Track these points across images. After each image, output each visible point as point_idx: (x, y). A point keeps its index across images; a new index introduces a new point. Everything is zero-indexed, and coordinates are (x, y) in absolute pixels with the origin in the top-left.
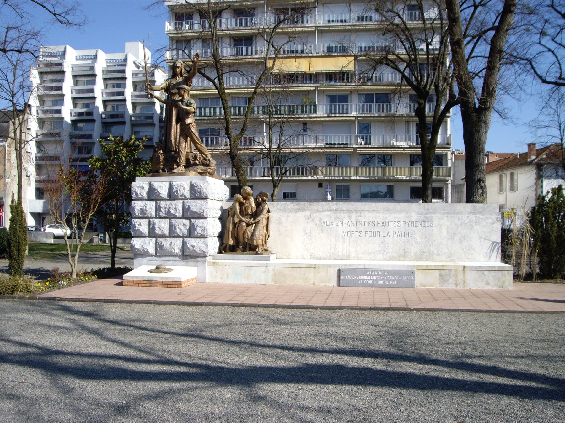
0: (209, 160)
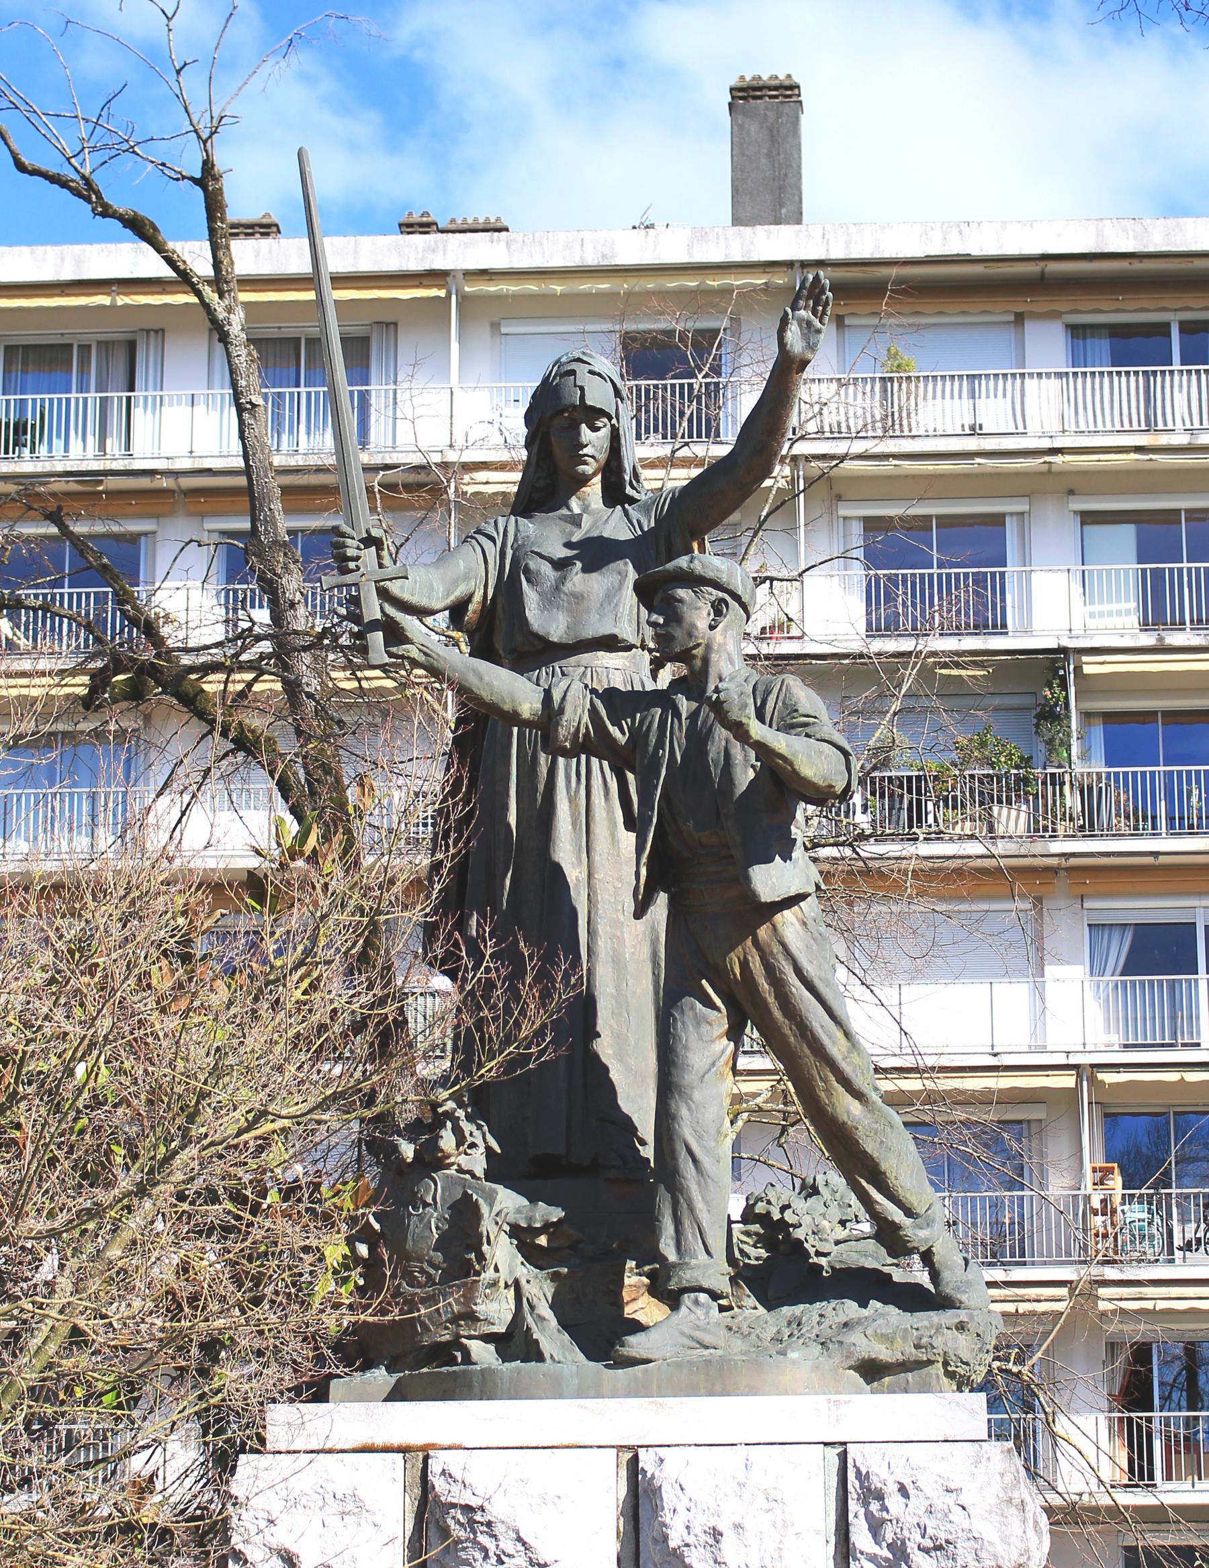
0: (927, 1258)
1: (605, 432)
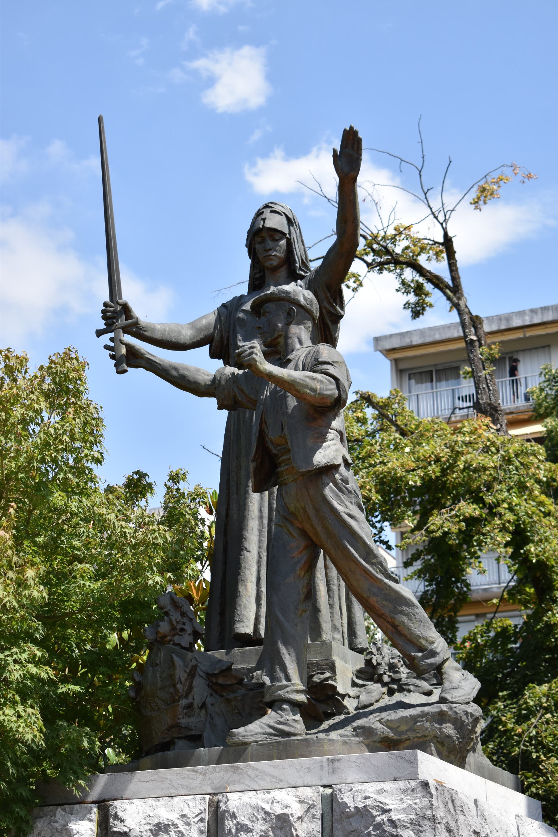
1: (283, 242)
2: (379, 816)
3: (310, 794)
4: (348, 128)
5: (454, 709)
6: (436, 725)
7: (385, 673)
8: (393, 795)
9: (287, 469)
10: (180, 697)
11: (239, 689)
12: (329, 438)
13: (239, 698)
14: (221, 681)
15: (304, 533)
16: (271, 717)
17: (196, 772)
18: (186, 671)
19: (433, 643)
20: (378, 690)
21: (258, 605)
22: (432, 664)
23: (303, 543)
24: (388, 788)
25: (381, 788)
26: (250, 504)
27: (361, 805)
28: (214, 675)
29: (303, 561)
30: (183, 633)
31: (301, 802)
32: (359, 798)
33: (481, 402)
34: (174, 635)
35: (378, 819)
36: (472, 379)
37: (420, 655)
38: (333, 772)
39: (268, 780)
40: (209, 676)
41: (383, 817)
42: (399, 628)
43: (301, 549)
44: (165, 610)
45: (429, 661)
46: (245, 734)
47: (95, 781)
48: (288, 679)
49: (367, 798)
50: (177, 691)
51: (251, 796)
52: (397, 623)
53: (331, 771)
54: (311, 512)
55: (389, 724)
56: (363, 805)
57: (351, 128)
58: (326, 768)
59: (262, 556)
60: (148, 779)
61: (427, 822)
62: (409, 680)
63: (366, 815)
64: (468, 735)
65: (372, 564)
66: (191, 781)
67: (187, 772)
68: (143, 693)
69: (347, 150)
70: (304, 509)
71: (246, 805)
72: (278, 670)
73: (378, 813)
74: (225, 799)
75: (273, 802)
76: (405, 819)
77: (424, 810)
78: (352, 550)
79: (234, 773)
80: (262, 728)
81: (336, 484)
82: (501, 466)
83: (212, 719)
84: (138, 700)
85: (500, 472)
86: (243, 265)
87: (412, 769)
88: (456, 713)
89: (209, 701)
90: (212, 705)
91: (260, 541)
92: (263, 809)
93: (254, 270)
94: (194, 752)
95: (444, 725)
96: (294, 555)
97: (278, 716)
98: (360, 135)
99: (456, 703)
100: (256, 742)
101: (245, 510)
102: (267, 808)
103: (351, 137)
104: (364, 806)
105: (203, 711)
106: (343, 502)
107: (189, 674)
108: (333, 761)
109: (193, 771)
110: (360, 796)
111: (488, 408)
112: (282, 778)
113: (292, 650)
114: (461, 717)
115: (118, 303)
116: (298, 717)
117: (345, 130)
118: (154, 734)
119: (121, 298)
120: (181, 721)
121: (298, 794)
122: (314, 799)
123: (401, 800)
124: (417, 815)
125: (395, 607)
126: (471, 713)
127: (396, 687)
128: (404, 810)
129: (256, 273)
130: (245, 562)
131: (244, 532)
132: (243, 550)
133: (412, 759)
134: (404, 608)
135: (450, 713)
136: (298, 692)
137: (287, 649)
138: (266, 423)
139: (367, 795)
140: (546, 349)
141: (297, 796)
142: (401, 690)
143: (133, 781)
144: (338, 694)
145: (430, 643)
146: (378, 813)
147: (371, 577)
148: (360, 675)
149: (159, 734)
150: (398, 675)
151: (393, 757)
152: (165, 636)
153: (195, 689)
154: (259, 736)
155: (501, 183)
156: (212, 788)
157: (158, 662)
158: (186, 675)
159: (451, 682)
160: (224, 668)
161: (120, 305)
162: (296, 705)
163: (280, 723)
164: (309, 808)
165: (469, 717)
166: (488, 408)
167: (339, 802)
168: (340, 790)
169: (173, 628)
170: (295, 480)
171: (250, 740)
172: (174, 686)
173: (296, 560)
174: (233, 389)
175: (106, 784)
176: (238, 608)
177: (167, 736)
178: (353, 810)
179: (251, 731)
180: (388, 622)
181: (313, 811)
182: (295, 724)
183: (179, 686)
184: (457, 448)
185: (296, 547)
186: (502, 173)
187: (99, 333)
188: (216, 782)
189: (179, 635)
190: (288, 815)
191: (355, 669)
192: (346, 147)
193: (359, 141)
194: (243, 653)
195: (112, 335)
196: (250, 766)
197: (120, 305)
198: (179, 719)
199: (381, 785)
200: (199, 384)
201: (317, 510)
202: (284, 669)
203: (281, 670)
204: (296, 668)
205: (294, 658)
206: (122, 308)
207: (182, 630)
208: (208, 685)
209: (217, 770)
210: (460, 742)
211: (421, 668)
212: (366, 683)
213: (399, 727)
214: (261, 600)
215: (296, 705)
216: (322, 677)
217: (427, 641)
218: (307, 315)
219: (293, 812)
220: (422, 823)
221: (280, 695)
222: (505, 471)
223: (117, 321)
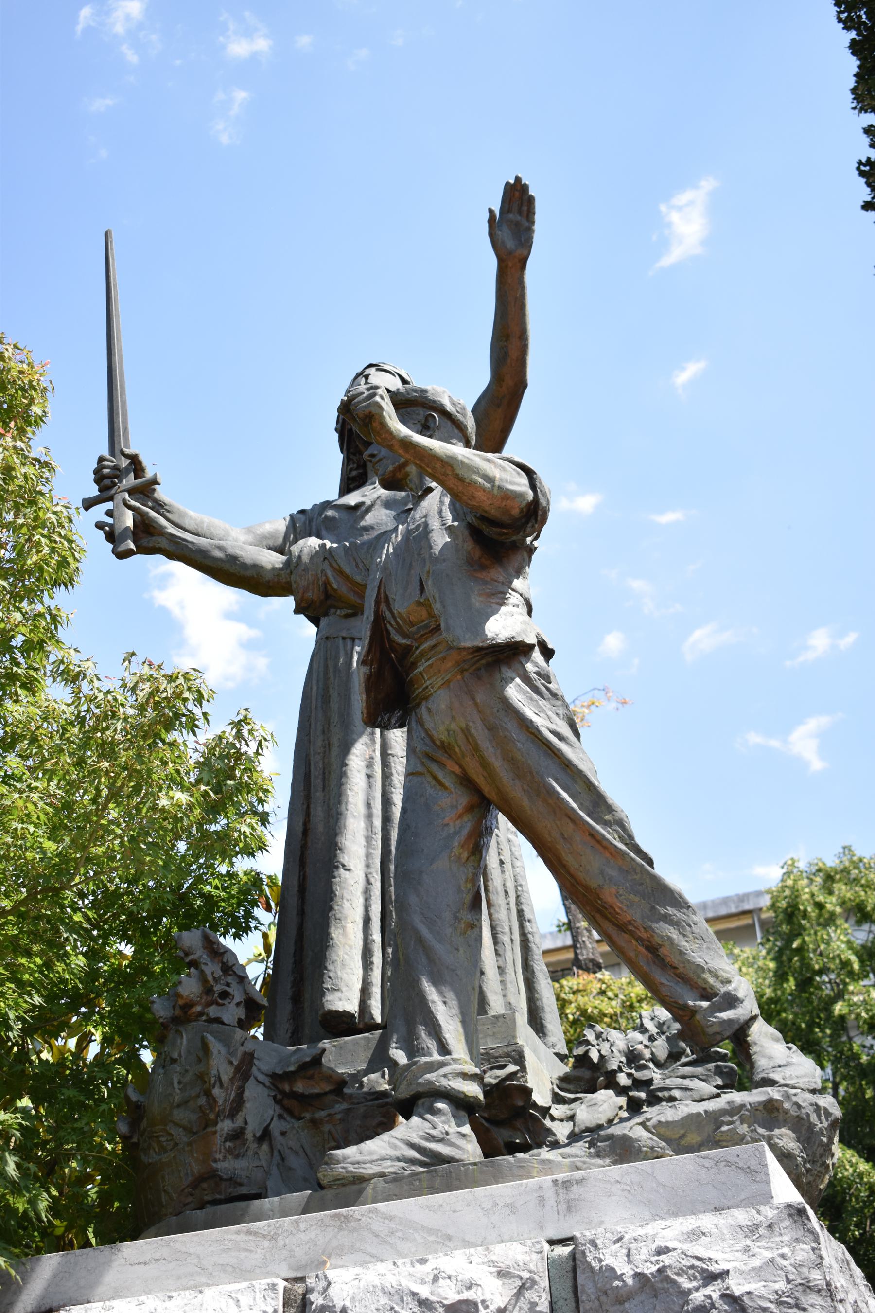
2: (697, 1289)
3: (521, 1258)
4: (512, 181)
5: (794, 1099)
6: (761, 1131)
7: (620, 1070)
8: (723, 1240)
9: (431, 666)
10: (218, 1115)
11: (337, 1102)
12: (511, 601)
13: (338, 1117)
14: (300, 1087)
15: (467, 782)
16: (411, 1129)
17: (255, 1234)
18: (231, 1063)
19: (729, 982)
20: (611, 1101)
21: (367, 964)
22: (730, 1021)
23: (463, 800)
24: (709, 1226)
25: (691, 1227)
26: (349, 792)
27: (650, 1269)
28: (288, 1076)
29: (465, 832)
30: (225, 1002)
31: (502, 1274)
32: (643, 1253)
33: (581, 958)
34: (209, 1004)
35: (698, 1297)
36: (568, 933)
37: (705, 1004)
38: (569, 1208)
39: (419, 1239)
40: (276, 1078)
41: (708, 1290)
42: (663, 951)
43: (461, 808)
44: (191, 957)
45: (725, 1015)
46: (359, 1158)
47: (32, 1270)
48: (444, 1049)
49: (662, 1251)
50: (212, 1101)
51: (382, 1271)
52: (658, 940)
53: (563, 1207)
54: (479, 733)
55: (662, 1130)
56: (654, 1269)
57: (518, 179)
58: (551, 1201)
59: (372, 880)
60: (147, 1257)
61: (814, 1298)
62: (668, 1081)
63: (666, 1291)
64: (821, 1156)
65: (606, 824)
66: (243, 1255)
67: (234, 1237)
68: (144, 1124)
69: (511, 216)
70: (466, 732)
71: (372, 1290)
72: (423, 1034)
73: (695, 1284)
74: (323, 1284)
75: (436, 1279)
76: (764, 1292)
77: (805, 1270)
78: (565, 795)
79: (341, 1229)
80: (395, 1147)
81: (527, 679)
82: (622, 1013)
83: (283, 1159)
84: (135, 1140)
85: (621, 1020)
86: (334, 459)
87: (755, 1186)
88: (799, 1107)
89: (276, 1127)
90: (283, 1134)
91: (368, 856)
92: (414, 1294)
93: (348, 465)
94: (248, 1207)
95: (777, 1131)
96: (446, 820)
97: (427, 1124)
98: (531, 192)
99: (794, 1088)
100: (382, 1175)
101: (340, 802)
102: (424, 1292)
103: (517, 194)
104: (659, 1271)
105: (265, 1147)
106: (543, 711)
107: (238, 1069)
108: (566, 1185)
109: (249, 1232)
110: (644, 1251)
111: (590, 965)
112: (449, 1232)
113: (450, 995)
114: (808, 1115)
115: (123, 453)
116: (467, 1129)
117: (507, 184)
118: (164, 1198)
119: (127, 446)
120: (219, 1165)
121: (494, 1258)
122: (532, 1267)
123: (747, 1249)
124: (789, 1281)
125: (653, 908)
126: (825, 1109)
127: (643, 1095)
128: (757, 1272)
129: (351, 470)
130: (342, 888)
131: (339, 839)
132: (337, 867)
133: (753, 1164)
134: (671, 911)
135: (786, 1105)
136: (465, 1076)
137: (441, 993)
138: (387, 598)
139: (662, 1244)
140: (616, 968)
141: (493, 1263)
142: (654, 1100)
143: (115, 1264)
144: (535, 1105)
145: (722, 983)
146: (695, 1284)
147: (605, 847)
148: (565, 1086)
149: (175, 1197)
150: (646, 1072)
151: (707, 1163)
152: (189, 1005)
153: (248, 1105)
154: (389, 1163)
155: (593, 707)
156: (291, 1268)
157: (175, 1055)
158: (231, 1070)
159: (770, 1058)
160: (308, 1059)
161: (127, 456)
162: (462, 1105)
163: (432, 1138)
164: (522, 1287)
165: (823, 1118)
166: (590, 965)
167: (592, 1269)
168: (593, 1243)
169: (208, 990)
170: (446, 684)
171: (371, 1172)
172: (208, 1093)
173: (452, 830)
174: (322, 571)
175: (55, 1276)
176: (330, 967)
177: (190, 1199)
178: (630, 1282)
179: (371, 1153)
180: (639, 939)
181: (529, 1295)
182: (461, 1142)
183: (216, 1091)
184: (563, 995)
185: (451, 802)
186: (593, 697)
187: (88, 504)
188: (299, 1252)
189: (219, 1004)
190: (475, 1304)
191: (556, 1076)
192: (509, 212)
193: (531, 200)
194: (341, 1047)
195: (109, 505)
196: (376, 1211)
197: (127, 456)
198: (215, 1161)
199: (690, 1223)
200: (262, 567)
201: (492, 729)
202: (436, 1031)
203: (429, 1034)
204: (461, 1030)
205: (455, 1011)
206: (130, 464)
207: (225, 995)
208: (275, 1097)
209: (303, 1226)
210: (808, 1170)
211: (711, 1031)
212: (579, 1095)
213: (683, 1136)
214: (372, 956)
215: (462, 1105)
216: (502, 1073)
217: (717, 977)
218: (456, 431)
219: (487, 1297)
220: (805, 1301)
221: (430, 1082)
222: (628, 1019)
223: (121, 481)
